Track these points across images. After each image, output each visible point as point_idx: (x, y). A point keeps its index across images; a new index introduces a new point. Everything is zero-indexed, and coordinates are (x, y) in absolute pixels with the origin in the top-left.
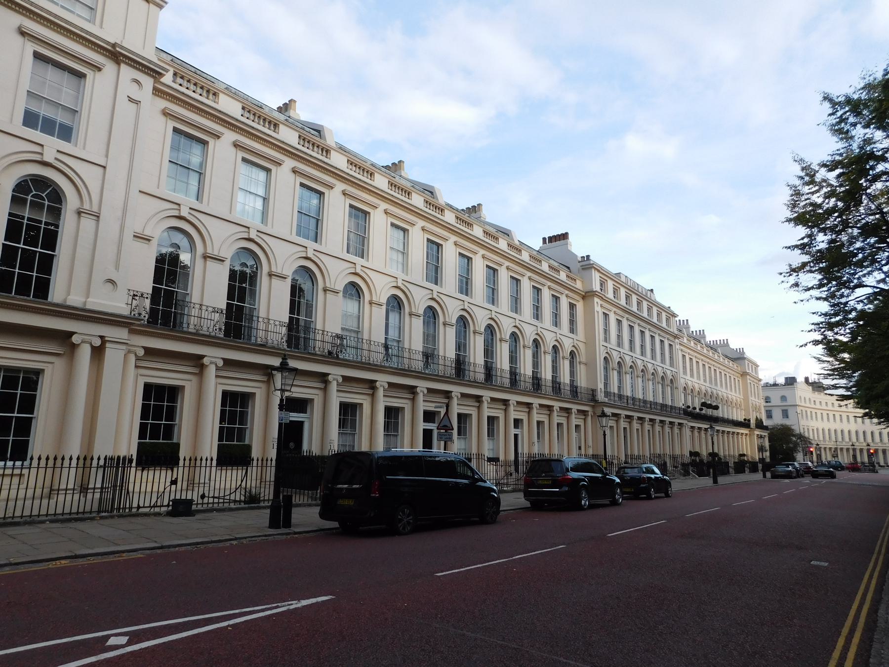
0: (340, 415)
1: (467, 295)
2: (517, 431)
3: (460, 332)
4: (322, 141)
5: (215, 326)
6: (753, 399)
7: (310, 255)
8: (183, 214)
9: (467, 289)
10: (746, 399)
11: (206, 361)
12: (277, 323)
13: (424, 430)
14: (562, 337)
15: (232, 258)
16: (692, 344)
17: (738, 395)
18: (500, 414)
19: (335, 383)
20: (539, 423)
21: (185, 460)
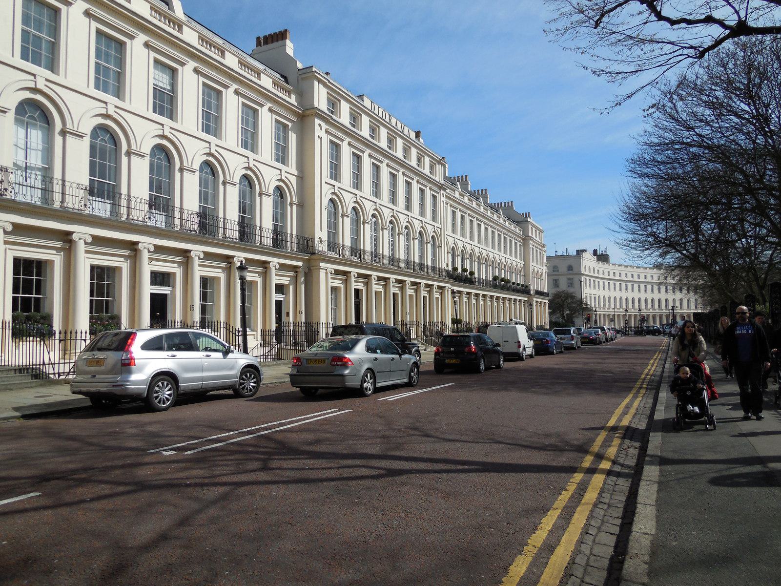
0: (92, 279)
1: (252, 151)
2: (280, 297)
3: (277, 202)
4: (170, 12)
5: (80, 202)
6: (534, 264)
7: (167, 133)
8: (109, 113)
9: (253, 145)
10: (526, 265)
11: (75, 237)
12: (74, 185)
13: (152, 294)
14: (457, 241)
15: (17, 109)
16: (466, 200)
17: (518, 260)
19: (82, 242)
20: (205, 281)
21: (81, 333)
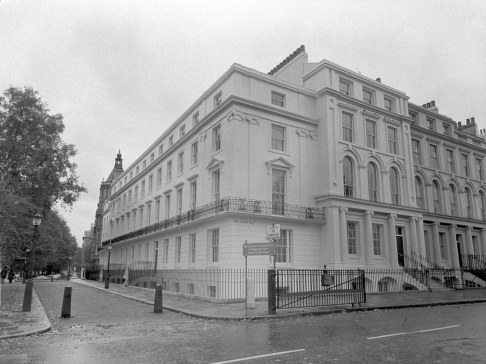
18: (447, 233)
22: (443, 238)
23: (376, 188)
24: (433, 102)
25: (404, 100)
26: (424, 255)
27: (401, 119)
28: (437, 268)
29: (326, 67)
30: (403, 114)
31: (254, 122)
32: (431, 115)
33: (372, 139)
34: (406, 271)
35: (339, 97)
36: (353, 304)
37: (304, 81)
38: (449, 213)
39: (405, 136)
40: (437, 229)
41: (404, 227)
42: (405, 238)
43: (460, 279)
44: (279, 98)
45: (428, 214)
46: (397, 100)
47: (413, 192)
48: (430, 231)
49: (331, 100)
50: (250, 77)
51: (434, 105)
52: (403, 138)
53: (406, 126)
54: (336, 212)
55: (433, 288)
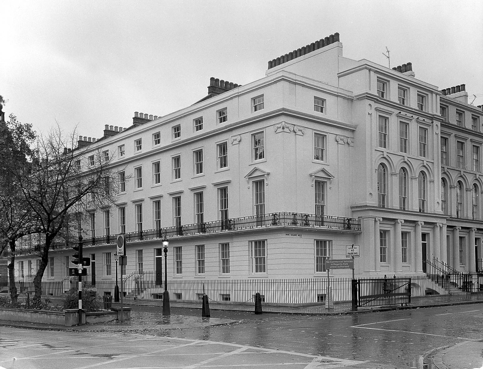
18: (467, 237)
20: (461, 238)
22: (463, 242)
23: (405, 195)
24: (464, 86)
25: (436, 95)
26: (445, 262)
27: (432, 118)
28: (455, 273)
29: (366, 68)
30: (435, 113)
31: (300, 133)
32: (461, 107)
33: (461, 157)
34: (429, 276)
35: (377, 101)
36: (402, 304)
37: (339, 77)
38: (470, 217)
39: (435, 136)
40: (458, 234)
41: (429, 233)
42: (429, 245)
43: (476, 284)
44: (320, 104)
45: (451, 219)
46: (430, 95)
47: (439, 197)
48: (451, 237)
49: (370, 105)
50: (295, 84)
51: (464, 89)
52: (433, 138)
53: (437, 125)
54: (372, 222)
55: (453, 292)
